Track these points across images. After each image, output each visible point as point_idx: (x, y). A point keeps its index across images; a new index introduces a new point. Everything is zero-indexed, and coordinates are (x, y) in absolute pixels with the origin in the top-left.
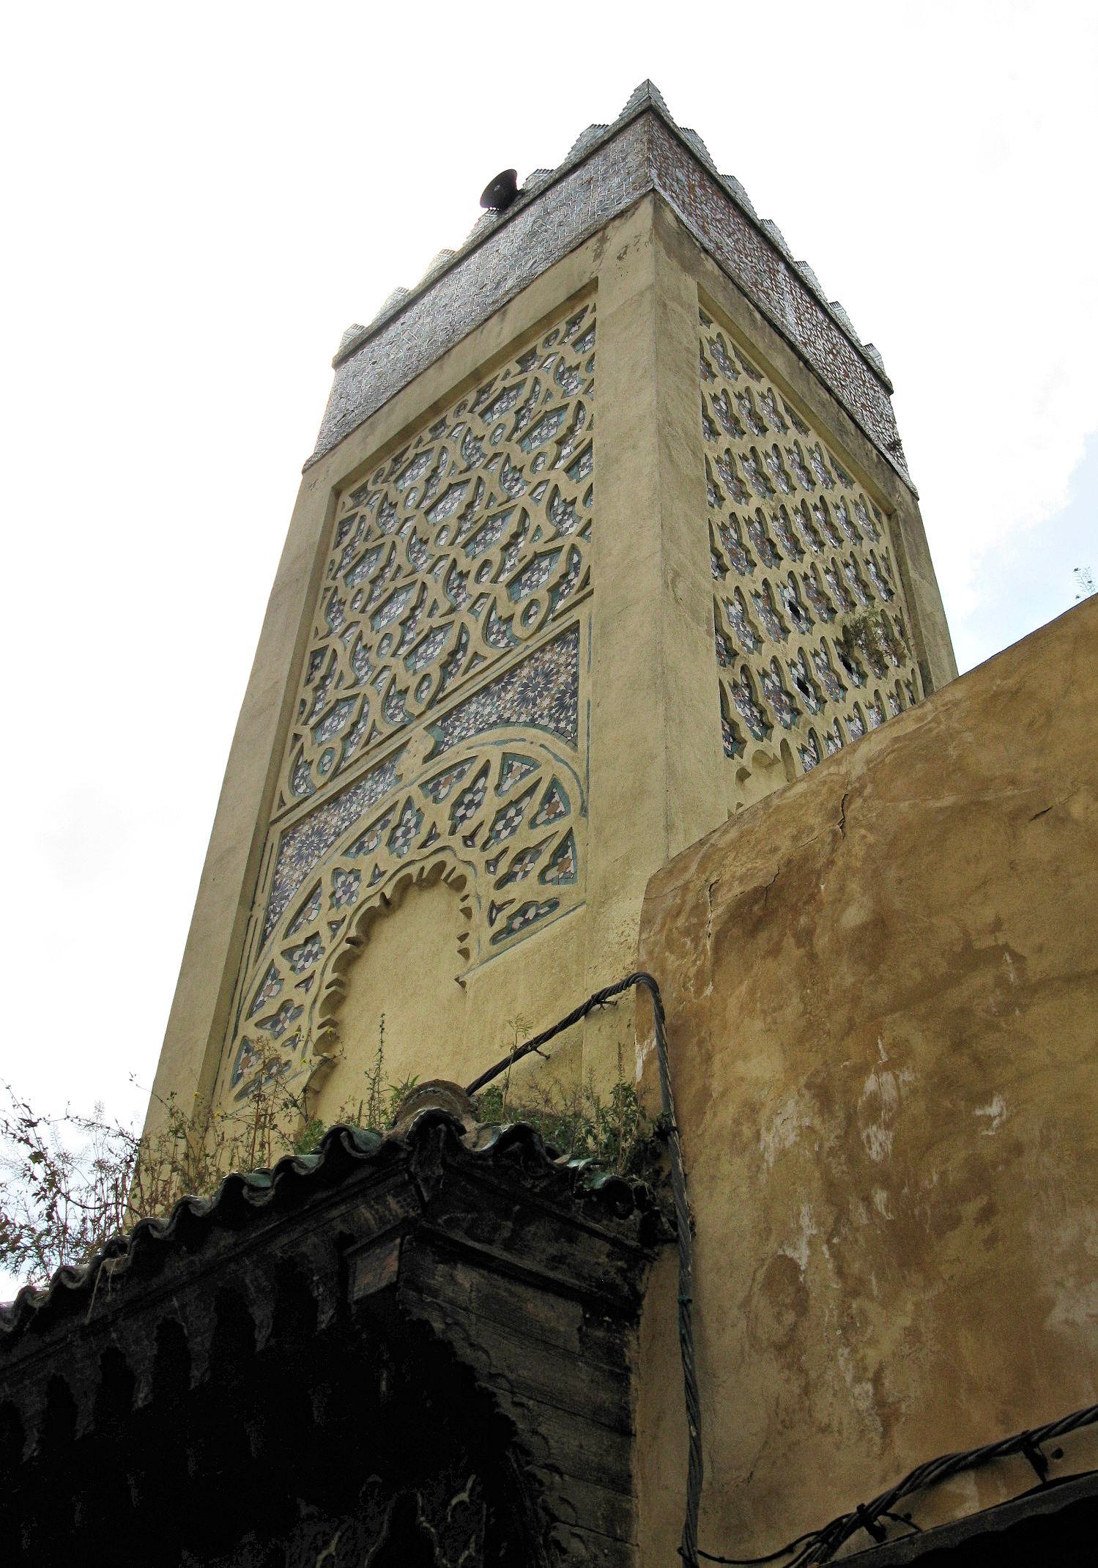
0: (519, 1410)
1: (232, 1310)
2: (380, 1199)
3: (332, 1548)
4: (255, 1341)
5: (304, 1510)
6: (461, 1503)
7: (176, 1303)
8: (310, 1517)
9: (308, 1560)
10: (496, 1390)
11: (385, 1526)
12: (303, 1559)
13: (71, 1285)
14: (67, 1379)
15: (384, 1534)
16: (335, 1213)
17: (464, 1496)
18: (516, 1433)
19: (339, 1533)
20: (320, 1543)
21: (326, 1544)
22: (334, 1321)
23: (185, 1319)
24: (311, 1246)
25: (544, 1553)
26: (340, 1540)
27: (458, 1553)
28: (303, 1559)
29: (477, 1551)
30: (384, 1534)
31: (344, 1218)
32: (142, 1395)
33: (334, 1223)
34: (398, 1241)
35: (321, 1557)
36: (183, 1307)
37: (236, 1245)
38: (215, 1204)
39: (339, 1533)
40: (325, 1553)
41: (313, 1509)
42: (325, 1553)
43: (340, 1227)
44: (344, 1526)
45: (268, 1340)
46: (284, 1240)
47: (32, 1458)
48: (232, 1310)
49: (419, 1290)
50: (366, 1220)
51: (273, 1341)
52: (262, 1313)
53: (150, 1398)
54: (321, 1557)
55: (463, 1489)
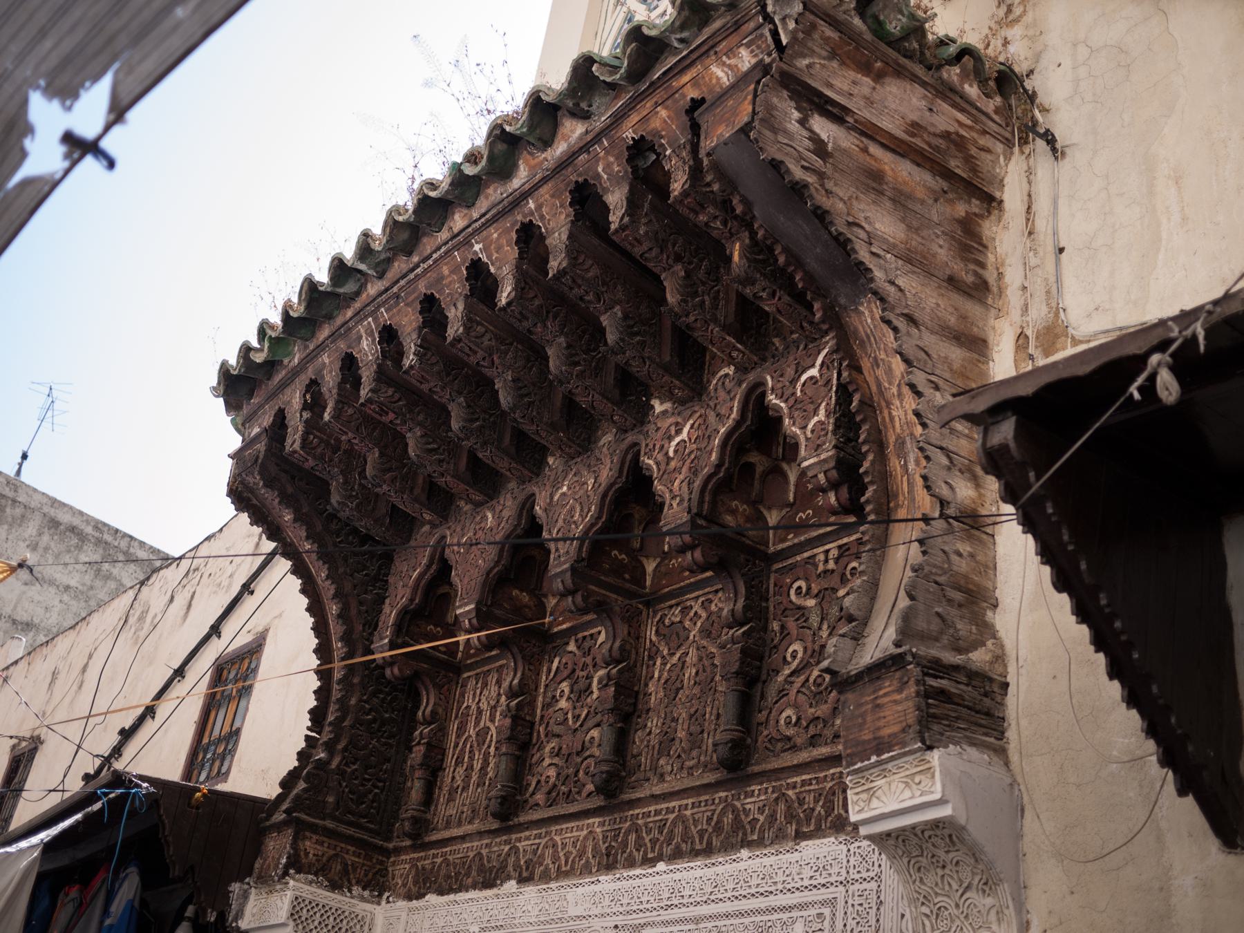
0: (876, 260)
1: (586, 199)
2: (730, 52)
3: (684, 435)
4: (606, 209)
5: (658, 407)
6: (812, 378)
7: (532, 205)
8: (665, 412)
9: (662, 447)
10: (853, 238)
11: (735, 409)
12: (657, 447)
13: (433, 194)
14: (437, 296)
15: (734, 416)
16: (686, 78)
17: (814, 372)
18: (872, 280)
19: (691, 421)
20: (673, 433)
21: (678, 432)
22: (686, 186)
23: (542, 217)
24: (662, 119)
25: (898, 403)
26: (692, 427)
27: (807, 419)
28: (657, 447)
29: (828, 416)
30: (734, 416)
31: (695, 82)
32: (505, 295)
33: (685, 89)
34: (752, 86)
35: (674, 443)
36: (539, 207)
37: (587, 132)
38: (566, 85)
39: (691, 421)
40: (678, 439)
41: (668, 406)
42: (678, 439)
43: (692, 93)
44: (698, 415)
45: (622, 219)
46: (634, 118)
47: (411, 367)
48: (586, 199)
49: (775, 131)
50: (718, 79)
51: (626, 219)
52: (616, 199)
53: (513, 294)
54: (674, 443)
55: (813, 366)
